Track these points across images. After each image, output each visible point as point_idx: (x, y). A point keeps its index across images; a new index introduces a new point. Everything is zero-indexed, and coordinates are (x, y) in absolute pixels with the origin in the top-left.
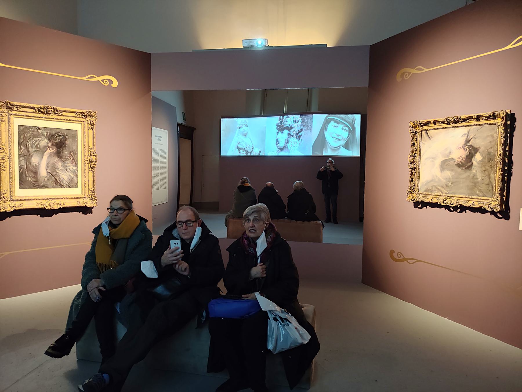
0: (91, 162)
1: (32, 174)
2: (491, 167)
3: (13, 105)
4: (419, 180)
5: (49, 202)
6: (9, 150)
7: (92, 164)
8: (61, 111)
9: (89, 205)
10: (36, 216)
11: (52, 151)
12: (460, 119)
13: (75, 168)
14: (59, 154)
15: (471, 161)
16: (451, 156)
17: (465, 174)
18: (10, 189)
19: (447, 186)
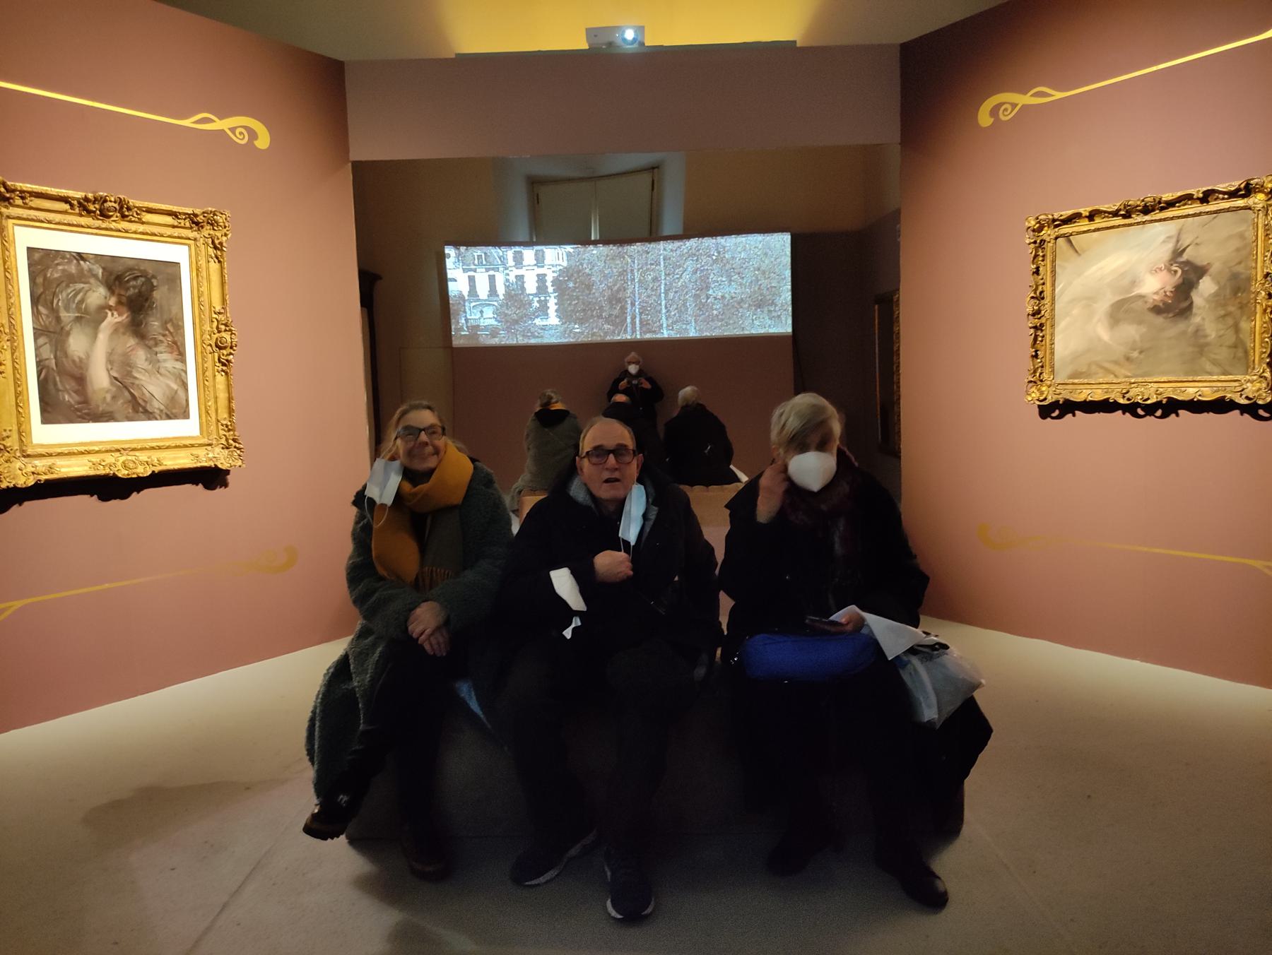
0: (220, 348)
1: (70, 385)
2: (1242, 307)
3: (13, 191)
4: (1052, 353)
5: (122, 459)
6: (10, 316)
7: (222, 353)
8: (139, 208)
9: (223, 465)
10: (86, 497)
11: (119, 319)
12: (1160, 203)
13: (179, 365)
14: (137, 328)
15: (1187, 297)
16: (1137, 291)
17: (1173, 329)
18: (19, 424)
19: (1128, 359)
